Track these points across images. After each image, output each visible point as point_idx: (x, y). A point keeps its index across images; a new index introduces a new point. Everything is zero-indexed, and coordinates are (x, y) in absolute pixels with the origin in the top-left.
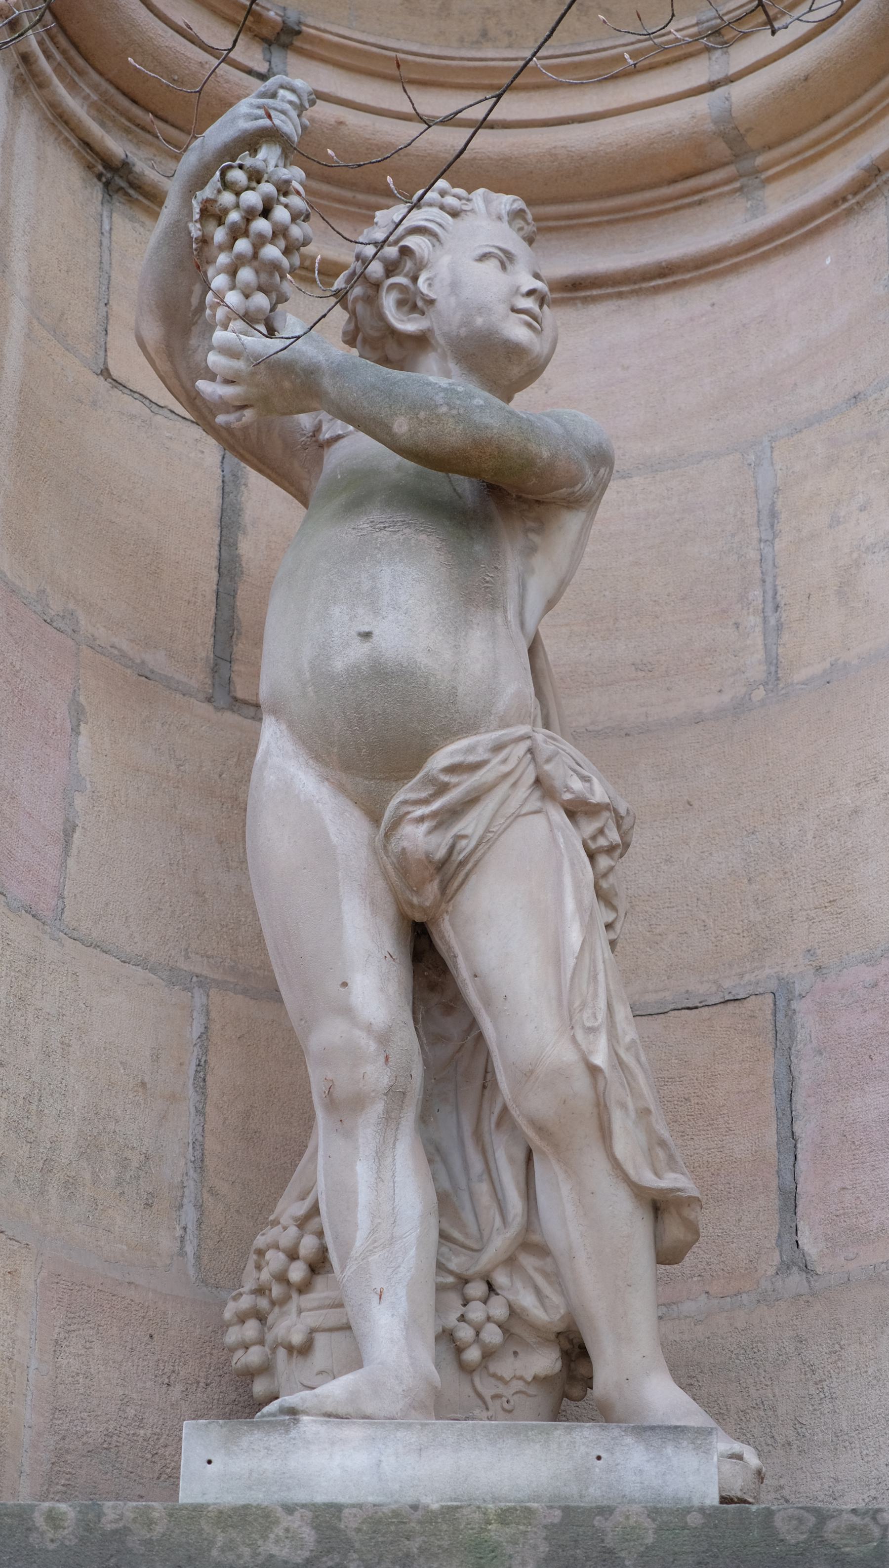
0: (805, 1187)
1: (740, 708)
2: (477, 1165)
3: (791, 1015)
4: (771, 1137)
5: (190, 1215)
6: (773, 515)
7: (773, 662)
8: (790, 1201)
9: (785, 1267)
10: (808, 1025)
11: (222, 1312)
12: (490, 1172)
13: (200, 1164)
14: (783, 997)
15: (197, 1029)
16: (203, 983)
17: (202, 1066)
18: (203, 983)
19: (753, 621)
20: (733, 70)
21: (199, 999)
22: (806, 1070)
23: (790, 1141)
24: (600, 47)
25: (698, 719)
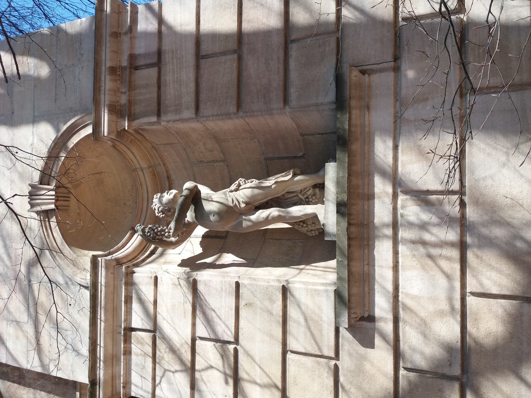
0: (293, 155)
1: (227, 166)
2: (289, 200)
3: (269, 158)
4: (286, 160)
5: (297, 241)
6: (201, 161)
7: (221, 161)
8: (295, 157)
9: (304, 158)
10: (271, 155)
11: (37, 81)
12: (290, 198)
13: (290, 240)
14: (266, 159)
15: (271, 240)
16: (265, 239)
17: (276, 239)
18: (265, 239)
19: (216, 164)
20: (390, 287)
21: (267, 240)
22: (277, 156)
23: (287, 158)
24: (146, 191)
25: (229, 172)
